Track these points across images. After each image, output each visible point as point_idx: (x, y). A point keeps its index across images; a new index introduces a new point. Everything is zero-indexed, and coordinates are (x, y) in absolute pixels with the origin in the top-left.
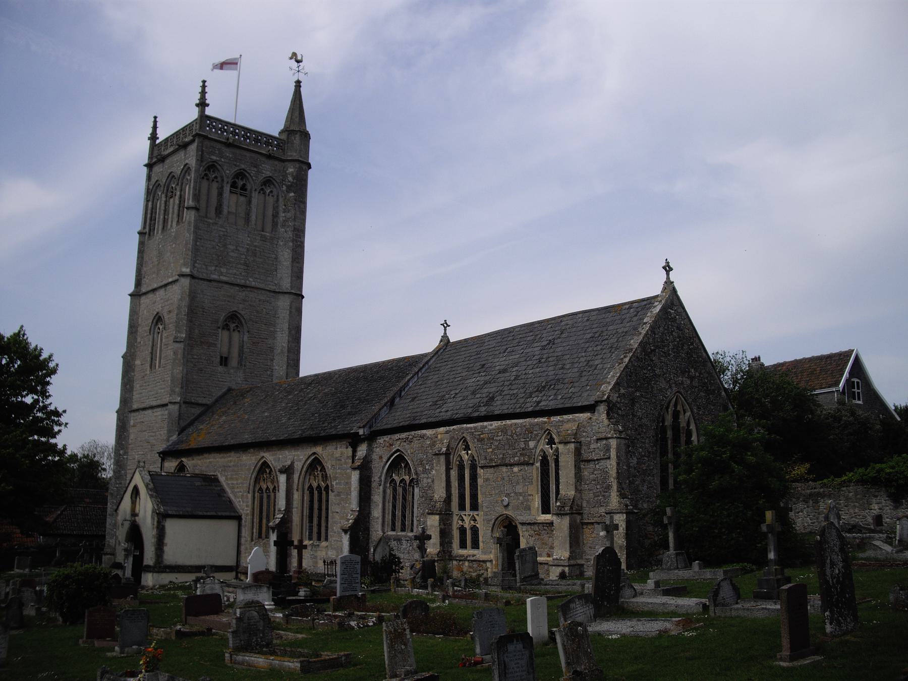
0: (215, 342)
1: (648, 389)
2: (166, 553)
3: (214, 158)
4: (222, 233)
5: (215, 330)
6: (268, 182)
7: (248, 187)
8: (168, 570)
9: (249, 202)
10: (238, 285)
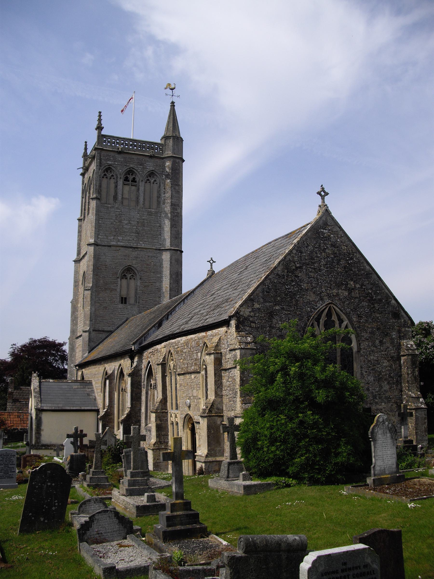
0: (116, 288)
1: (292, 302)
2: (42, 436)
3: (110, 163)
4: (118, 213)
5: (115, 280)
6: (152, 174)
7: (137, 179)
8: (44, 448)
9: (138, 189)
10: (131, 247)
